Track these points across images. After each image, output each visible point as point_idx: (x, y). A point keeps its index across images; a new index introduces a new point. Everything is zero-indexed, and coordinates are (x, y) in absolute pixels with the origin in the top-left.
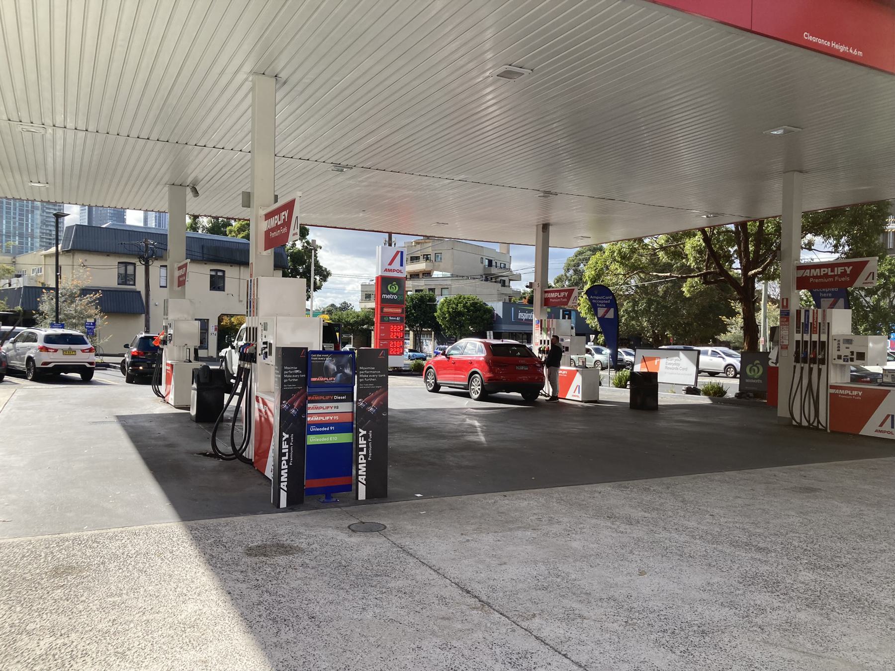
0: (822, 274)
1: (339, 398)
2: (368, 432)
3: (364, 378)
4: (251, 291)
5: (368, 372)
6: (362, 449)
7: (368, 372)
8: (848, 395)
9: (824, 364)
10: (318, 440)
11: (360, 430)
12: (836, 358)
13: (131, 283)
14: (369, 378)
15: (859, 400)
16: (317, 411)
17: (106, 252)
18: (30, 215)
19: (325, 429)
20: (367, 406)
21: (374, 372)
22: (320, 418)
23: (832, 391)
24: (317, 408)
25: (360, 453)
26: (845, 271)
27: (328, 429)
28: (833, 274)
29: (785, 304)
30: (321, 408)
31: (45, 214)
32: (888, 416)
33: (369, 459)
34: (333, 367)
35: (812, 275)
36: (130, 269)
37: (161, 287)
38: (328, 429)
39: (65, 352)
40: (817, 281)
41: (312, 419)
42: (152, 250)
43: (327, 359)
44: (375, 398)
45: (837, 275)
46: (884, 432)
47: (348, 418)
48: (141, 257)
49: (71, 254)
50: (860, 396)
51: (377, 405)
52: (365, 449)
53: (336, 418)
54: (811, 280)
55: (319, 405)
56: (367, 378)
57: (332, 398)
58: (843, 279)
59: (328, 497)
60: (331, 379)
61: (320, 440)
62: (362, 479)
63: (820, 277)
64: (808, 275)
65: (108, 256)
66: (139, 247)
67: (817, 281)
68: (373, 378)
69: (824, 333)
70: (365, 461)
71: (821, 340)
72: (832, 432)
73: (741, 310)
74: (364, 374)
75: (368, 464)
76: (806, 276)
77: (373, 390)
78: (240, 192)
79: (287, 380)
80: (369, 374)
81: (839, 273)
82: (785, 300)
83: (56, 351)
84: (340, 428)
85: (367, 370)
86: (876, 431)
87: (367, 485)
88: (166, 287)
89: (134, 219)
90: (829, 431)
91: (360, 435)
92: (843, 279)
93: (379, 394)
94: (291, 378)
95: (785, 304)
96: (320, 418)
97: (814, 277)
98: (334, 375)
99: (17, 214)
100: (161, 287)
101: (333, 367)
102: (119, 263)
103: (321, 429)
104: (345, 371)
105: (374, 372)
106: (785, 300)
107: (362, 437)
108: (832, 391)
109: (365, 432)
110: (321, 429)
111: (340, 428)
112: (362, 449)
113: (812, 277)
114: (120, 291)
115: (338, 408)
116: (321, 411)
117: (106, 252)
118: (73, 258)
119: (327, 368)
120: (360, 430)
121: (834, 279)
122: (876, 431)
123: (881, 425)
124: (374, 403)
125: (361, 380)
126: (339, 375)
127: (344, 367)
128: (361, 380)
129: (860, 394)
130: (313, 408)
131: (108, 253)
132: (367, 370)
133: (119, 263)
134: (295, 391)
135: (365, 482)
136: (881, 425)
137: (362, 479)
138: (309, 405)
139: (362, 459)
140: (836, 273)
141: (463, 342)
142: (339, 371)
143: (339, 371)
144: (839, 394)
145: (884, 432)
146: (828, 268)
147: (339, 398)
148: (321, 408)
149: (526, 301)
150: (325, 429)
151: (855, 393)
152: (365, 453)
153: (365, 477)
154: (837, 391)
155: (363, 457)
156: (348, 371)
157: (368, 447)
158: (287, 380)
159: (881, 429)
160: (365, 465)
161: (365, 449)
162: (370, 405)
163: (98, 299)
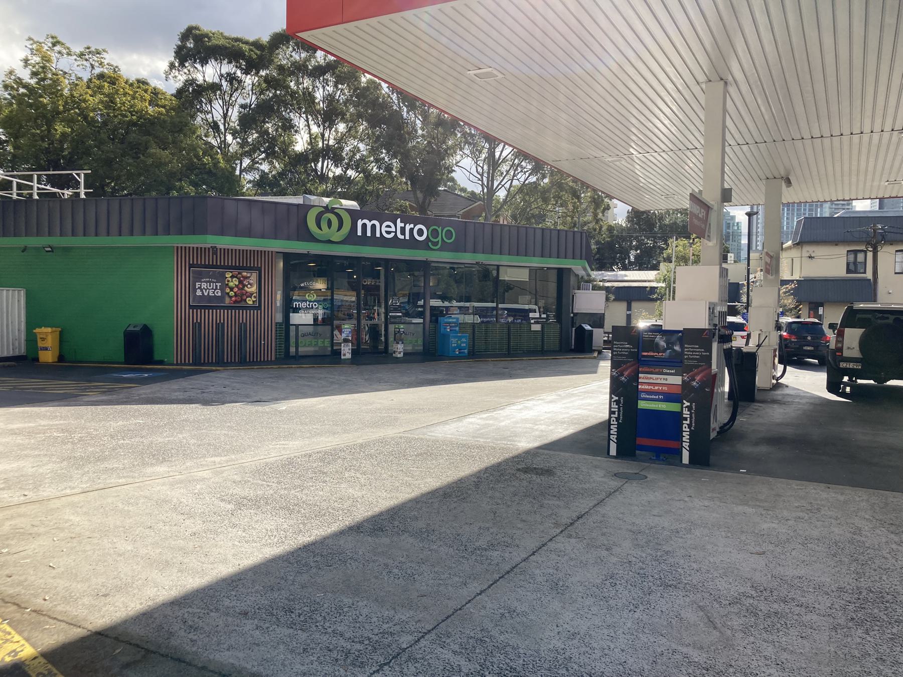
1: (668, 371)
2: (619, 398)
3: (617, 351)
5: (692, 350)
6: (686, 419)
7: (692, 350)
10: (648, 405)
11: (684, 401)
13: (862, 271)
14: (693, 355)
16: (648, 380)
17: (834, 242)
18: (819, 210)
19: (655, 397)
20: (690, 380)
21: (698, 350)
22: (650, 387)
24: (647, 378)
25: (684, 422)
27: (657, 397)
30: (651, 378)
31: (834, 206)
33: (693, 429)
34: (663, 344)
36: (860, 257)
37: (896, 273)
38: (657, 397)
41: (643, 387)
42: (881, 235)
43: (658, 337)
44: (626, 369)
47: (678, 391)
48: (868, 243)
49: (800, 246)
51: (628, 376)
52: (617, 412)
53: (665, 388)
55: (649, 376)
56: (691, 355)
57: (661, 370)
59: (658, 457)
60: (661, 354)
61: (650, 406)
62: (686, 445)
63: (394, 242)
65: (836, 245)
66: (867, 233)
68: (697, 355)
70: (688, 430)
74: (617, 348)
75: (692, 434)
76: (689, 446)
77: (697, 367)
78: (734, 187)
79: (687, 357)
80: (692, 352)
84: (669, 397)
85: (692, 348)
87: (618, 444)
89: (862, 206)
91: (684, 406)
93: (702, 371)
94: (691, 355)
96: (650, 387)
98: (664, 351)
99: (807, 210)
100: (896, 273)
101: (663, 344)
102: (848, 251)
103: (650, 397)
104: (675, 348)
105: (698, 350)
107: (685, 407)
109: (689, 404)
110: (650, 397)
111: (669, 397)
112: (686, 419)
114: (851, 280)
115: (666, 380)
116: (651, 381)
117: (834, 242)
118: (802, 250)
119: (657, 345)
120: (684, 401)
124: (698, 378)
125: (614, 353)
126: (668, 351)
127: (673, 344)
128: (614, 353)
130: (643, 378)
131: (836, 243)
132: (692, 348)
133: (848, 251)
134: (625, 363)
137: (686, 445)
138: (640, 375)
139: (613, 421)
140: (689, 416)
142: (668, 348)
143: (668, 348)
147: (668, 371)
148: (651, 378)
150: (655, 397)
152: (688, 422)
153: (616, 436)
156: (677, 348)
157: (619, 411)
158: (687, 357)
160: (616, 426)
161: (617, 412)
162: (622, 375)
163: (792, 289)
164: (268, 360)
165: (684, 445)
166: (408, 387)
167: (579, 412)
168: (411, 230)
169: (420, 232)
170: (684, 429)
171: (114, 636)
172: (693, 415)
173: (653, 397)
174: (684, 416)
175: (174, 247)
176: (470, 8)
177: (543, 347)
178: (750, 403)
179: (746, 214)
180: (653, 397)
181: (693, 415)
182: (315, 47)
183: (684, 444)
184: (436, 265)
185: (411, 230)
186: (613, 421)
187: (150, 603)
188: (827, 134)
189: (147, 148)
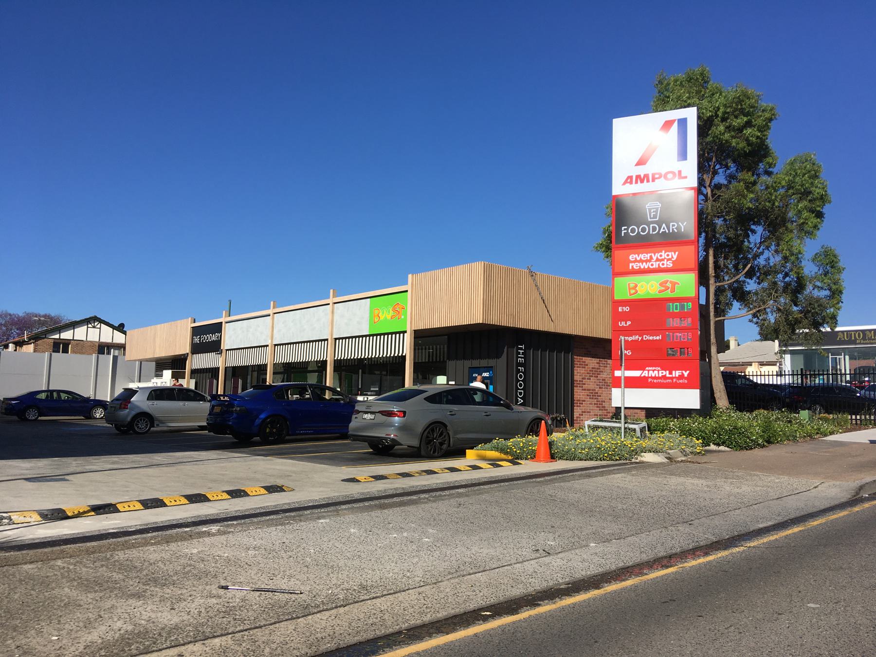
0: (660, 375)
4: (168, 363)
6: (671, 373)
8: (664, 377)
11: (688, 372)
25: (668, 372)
26: (683, 374)
28: (671, 376)
35: (650, 376)
39: (606, 590)
40: (655, 381)
45: (675, 377)
50: (686, 378)
54: (650, 380)
58: (681, 381)
63: (659, 378)
64: (647, 375)
67: (655, 381)
76: (644, 376)
81: (677, 376)
83: (653, 371)
88: (227, 350)
91: (684, 372)
92: (681, 381)
97: (655, 378)
107: (682, 373)
112: (671, 373)
113: (650, 377)
120: (688, 372)
121: (673, 381)
135: (642, 376)
139: (662, 373)
140: (674, 376)
141: (802, 412)
144: (648, 377)
146: (666, 371)
149: (723, 189)
155: (664, 374)
164: (371, 363)
165: (645, 371)
166: (361, 360)
168: (659, 264)
169: (627, 309)
174: (674, 372)
175: (185, 369)
177: (785, 377)
182: (66, 341)
184: (336, 364)
185: (659, 264)
186: (662, 373)
188: (767, 377)
189: (717, 189)
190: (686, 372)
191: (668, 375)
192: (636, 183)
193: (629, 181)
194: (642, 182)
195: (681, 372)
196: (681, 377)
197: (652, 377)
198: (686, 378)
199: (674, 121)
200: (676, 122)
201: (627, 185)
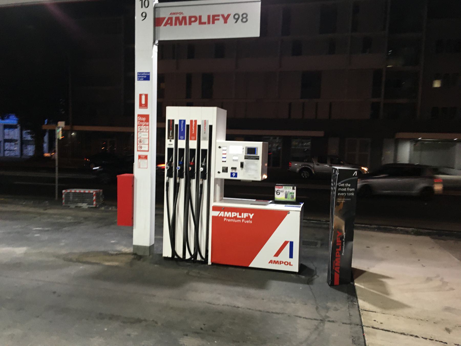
0: (233, 216)
6: (240, 215)
8: (235, 218)
9: (204, 178)
12: (221, 171)
15: (249, 224)
23: (216, 213)
25: (238, 214)
28: (240, 217)
29: (143, 102)
32: (286, 243)
40: (229, 220)
45: (243, 218)
46: (281, 263)
50: (251, 220)
54: (225, 219)
58: (248, 222)
63: (231, 218)
64: (223, 215)
67: (229, 220)
69: (205, 139)
71: (156, 17)
72: (213, 264)
73: (248, 214)
76: (221, 216)
81: (245, 217)
82: (143, 97)
86: (271, 262)
90: (210, 263)
91: (250, 214)
92: (248, 222)
95: (143, 102)
97: (229, 218)
106: (143, 97)
107: (249, 215)
108: (216, 213)
112: (240, 215)
120: (253, 215)
121: (241, 221)
122: (271, 262)
123: (277, 255)
129: (251, 216)
135: (220, 215)
136: (277, 255)
140: (243, 217)
144: (224, 217)
145: (281, 263)
151: (245, 215)
154: (222, 214)
155: (236, 215)
159: (276, 259)
167: (326, 172)
170: (233, 213)
171: (417, 318)
172: (239, 221)
173: (182, 126)
174: (243, 214)
176: (369, 311)
178: (150, 245)
179: (319, 328)
180: (182, 126)
181: (239, 221)
183: (222, 213)
186: (234, 214)
187: (399, 153)
190: (251, 214)
191: (238, 216)
192: (176, 24)
193: (169, 22)
194: (181, 24)
195: (248, 214)
196: (248, 218)
197: (226, 217)
198: (251, 220)
199: (288, 242)
200: (289, 243)
201: (168, 26)
